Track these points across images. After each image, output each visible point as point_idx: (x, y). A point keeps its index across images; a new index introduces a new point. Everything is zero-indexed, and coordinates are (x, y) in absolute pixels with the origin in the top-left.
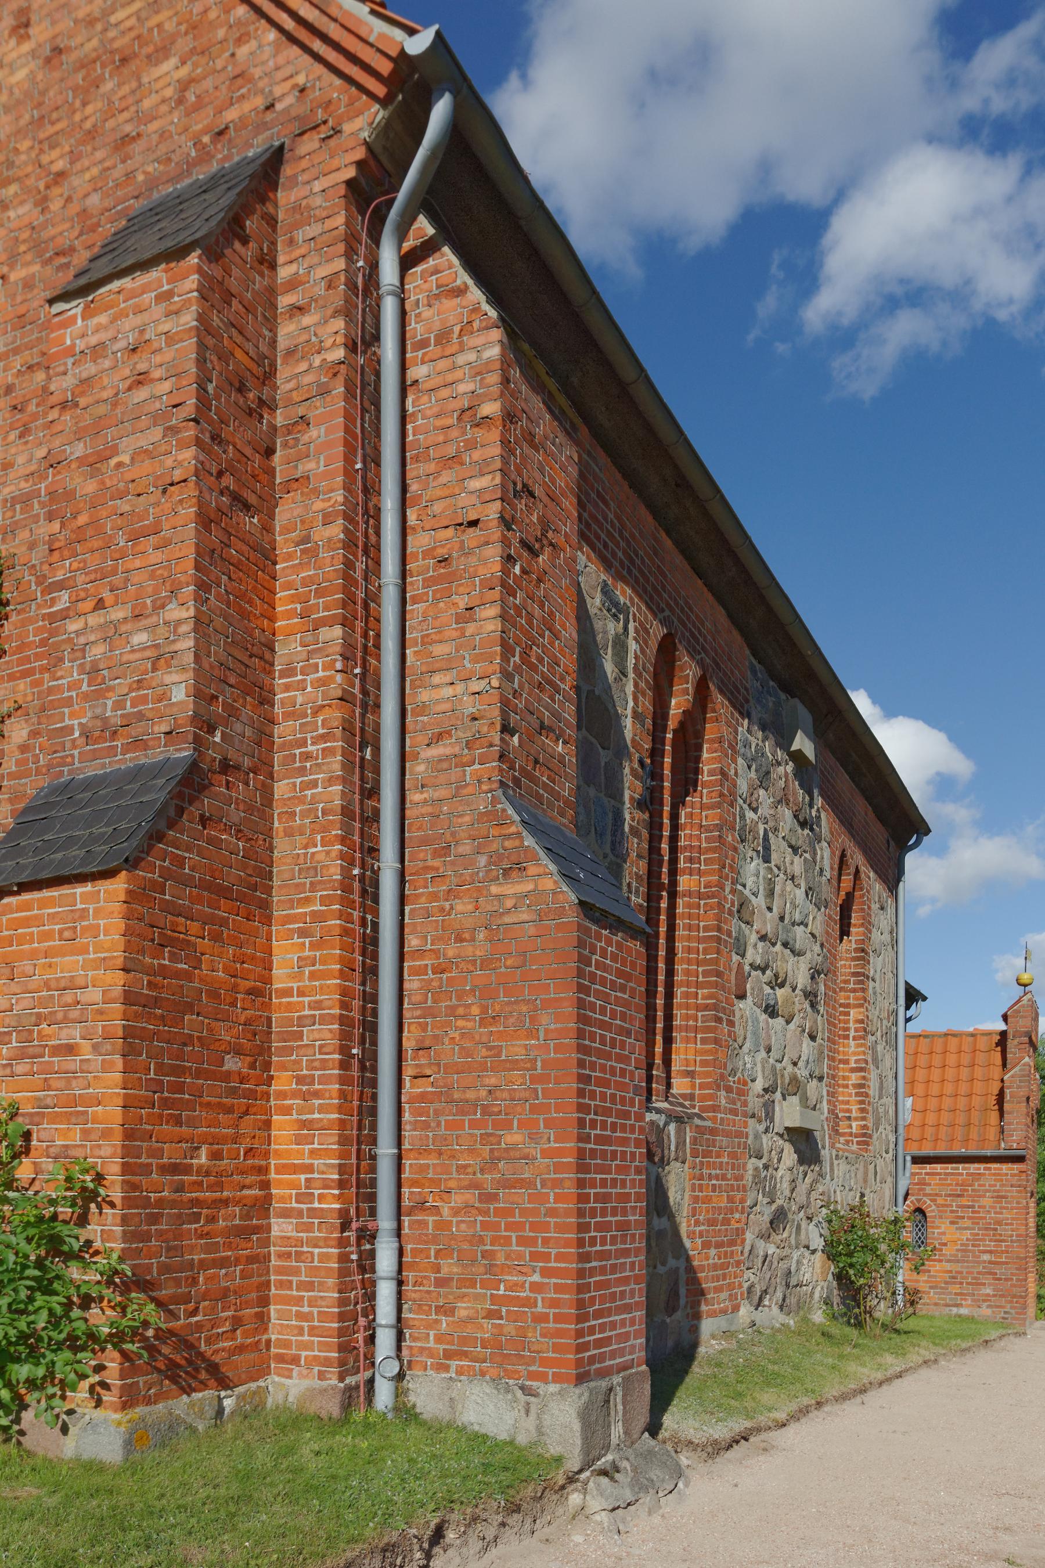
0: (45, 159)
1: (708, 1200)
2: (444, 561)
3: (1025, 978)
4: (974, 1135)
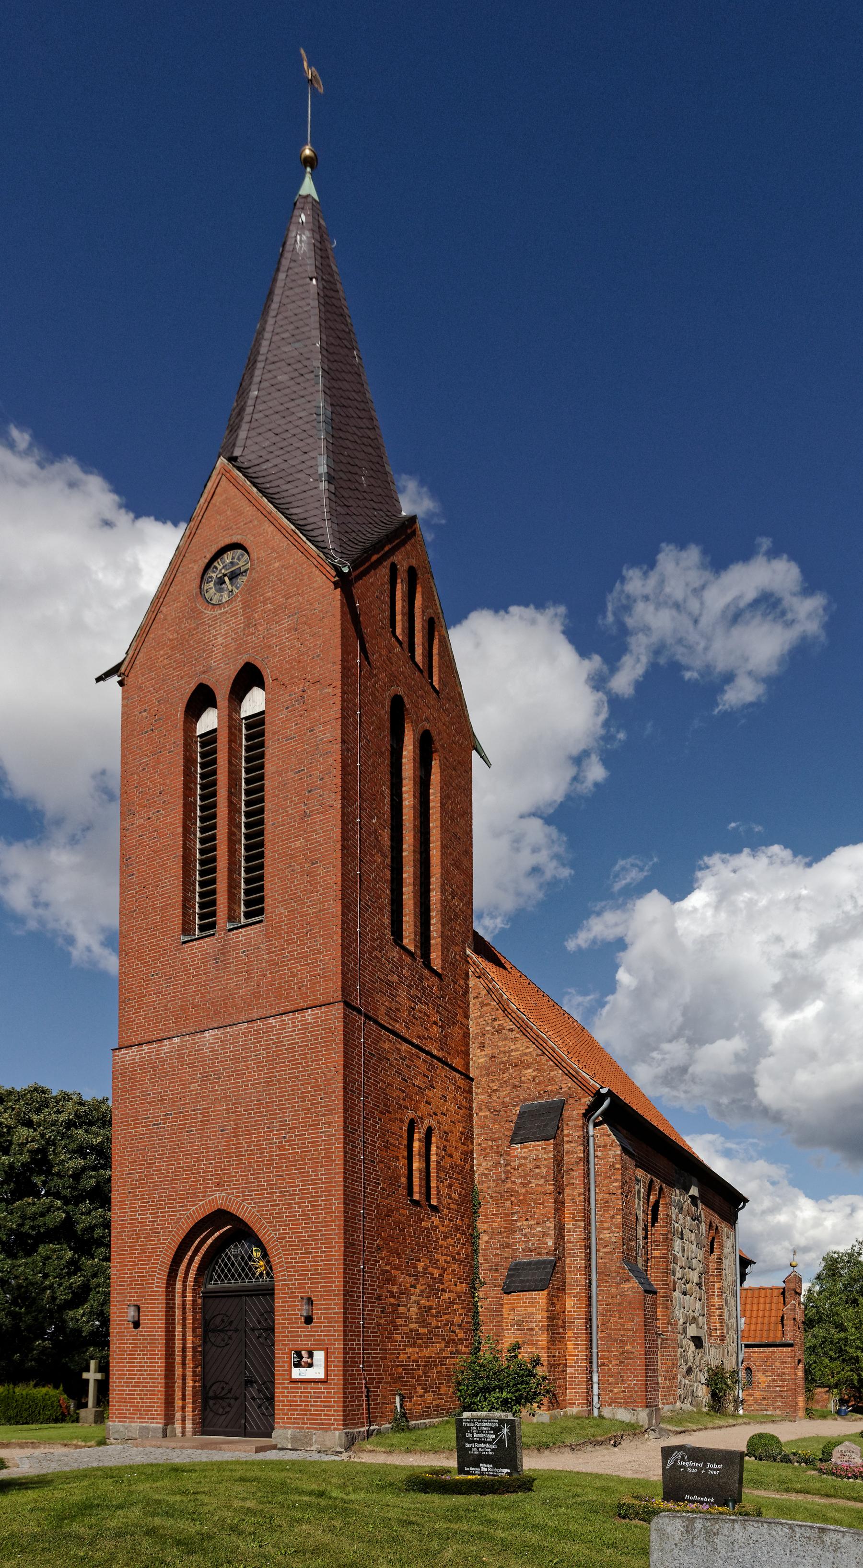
0: (491, 1085)
1: (665, 1363)
2: (607, 1202)
3: (794, 1263)
4: (772, 1335)
